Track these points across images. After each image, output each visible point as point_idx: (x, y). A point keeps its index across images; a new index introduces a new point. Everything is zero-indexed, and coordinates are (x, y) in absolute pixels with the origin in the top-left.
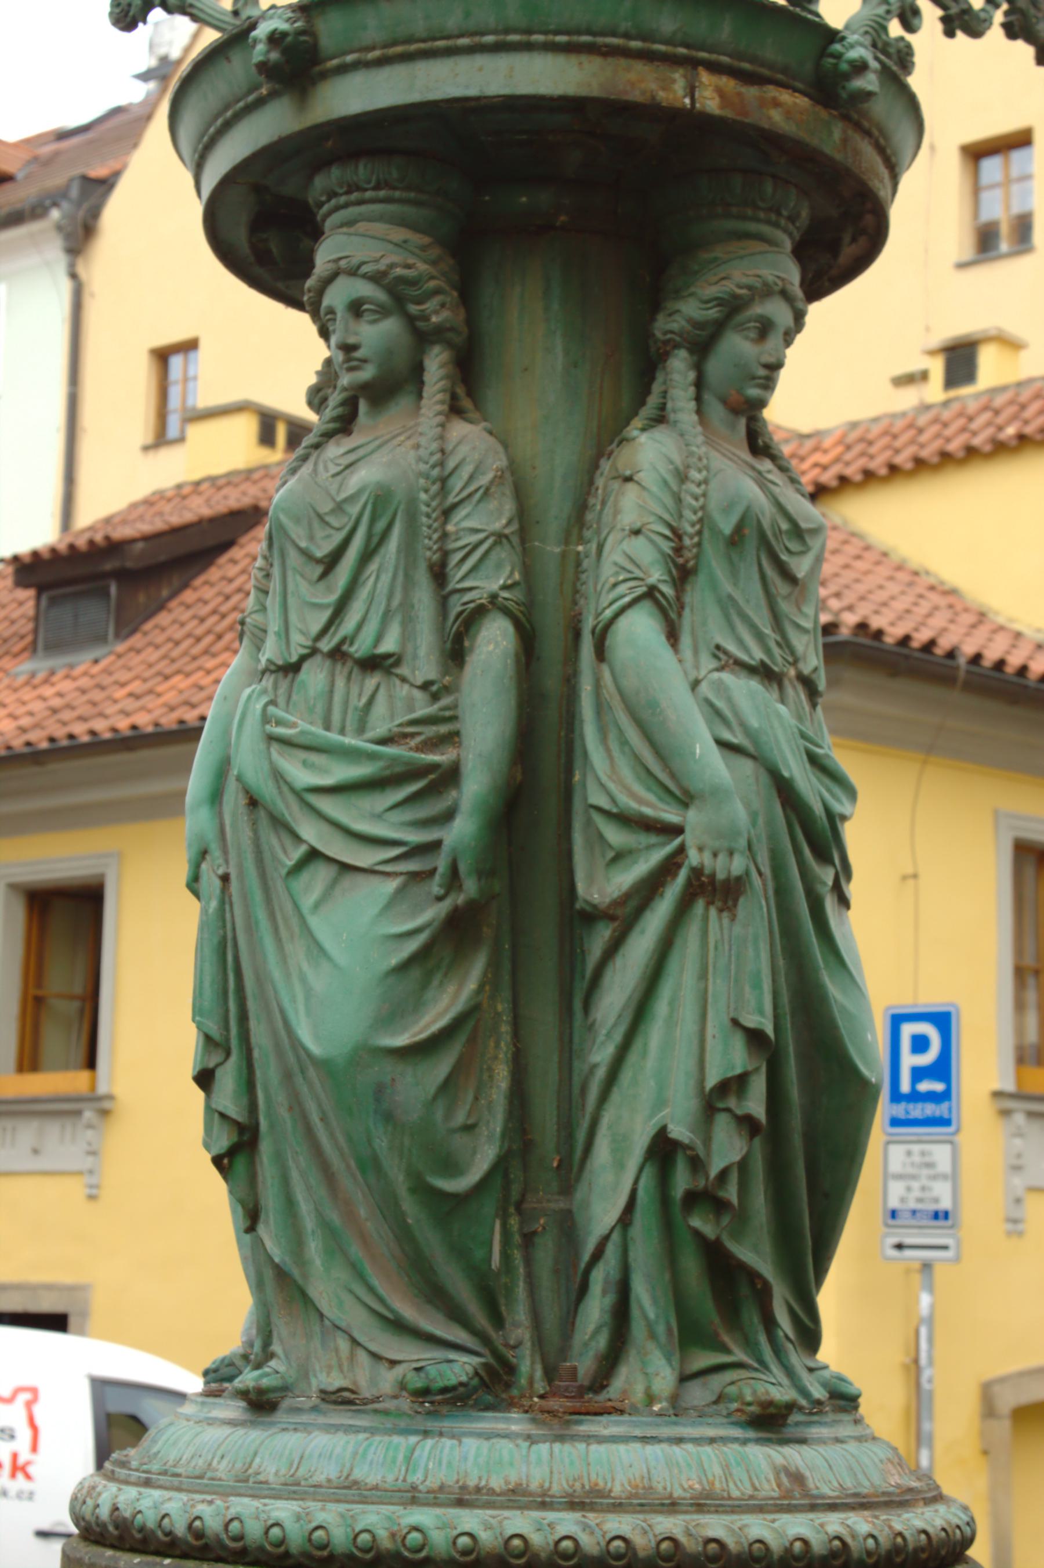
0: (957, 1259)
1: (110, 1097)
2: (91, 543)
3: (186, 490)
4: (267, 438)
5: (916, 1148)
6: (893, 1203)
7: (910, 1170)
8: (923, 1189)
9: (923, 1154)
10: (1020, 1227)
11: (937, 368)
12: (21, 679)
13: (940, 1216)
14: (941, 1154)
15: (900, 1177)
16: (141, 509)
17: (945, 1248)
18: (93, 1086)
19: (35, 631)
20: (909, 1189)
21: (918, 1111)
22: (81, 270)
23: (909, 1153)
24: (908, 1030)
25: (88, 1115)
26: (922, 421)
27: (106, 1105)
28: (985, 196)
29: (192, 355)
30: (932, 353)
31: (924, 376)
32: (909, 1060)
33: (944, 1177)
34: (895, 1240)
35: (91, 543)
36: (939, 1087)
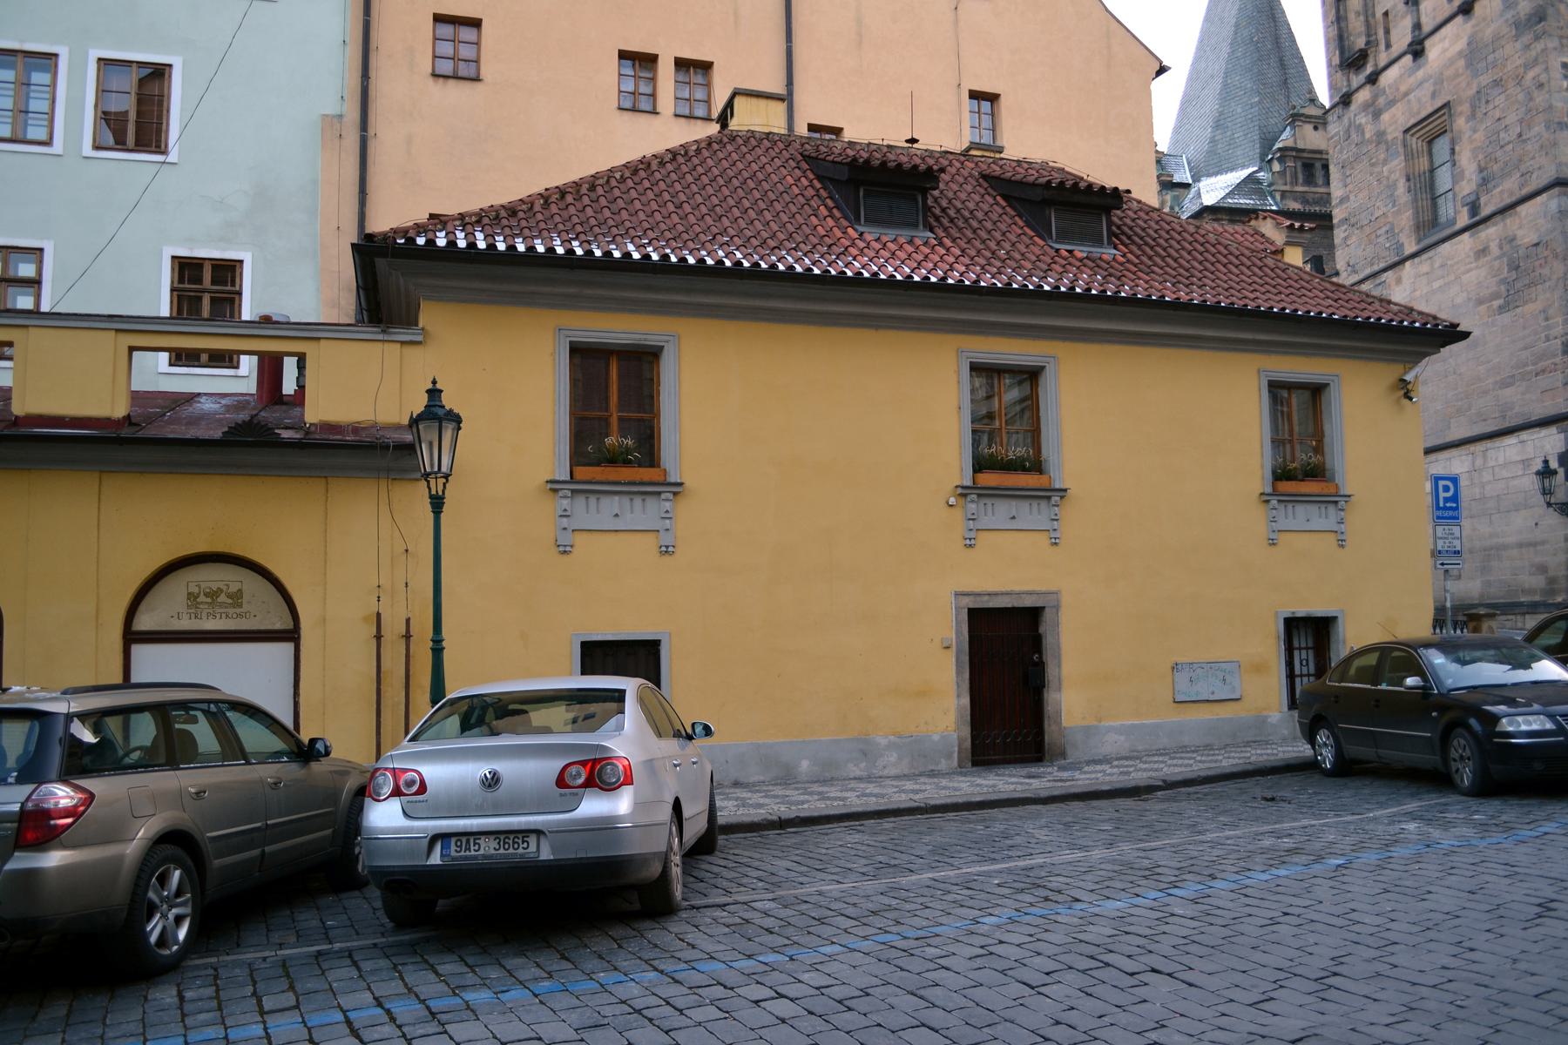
2: (884, 164)
6: (1439, 548)
14: (1456, 530)
15: (1441, 538)
24: (1441, 483)
32: (1442, 495)
35: (884, 164)
36: (1454, 505)
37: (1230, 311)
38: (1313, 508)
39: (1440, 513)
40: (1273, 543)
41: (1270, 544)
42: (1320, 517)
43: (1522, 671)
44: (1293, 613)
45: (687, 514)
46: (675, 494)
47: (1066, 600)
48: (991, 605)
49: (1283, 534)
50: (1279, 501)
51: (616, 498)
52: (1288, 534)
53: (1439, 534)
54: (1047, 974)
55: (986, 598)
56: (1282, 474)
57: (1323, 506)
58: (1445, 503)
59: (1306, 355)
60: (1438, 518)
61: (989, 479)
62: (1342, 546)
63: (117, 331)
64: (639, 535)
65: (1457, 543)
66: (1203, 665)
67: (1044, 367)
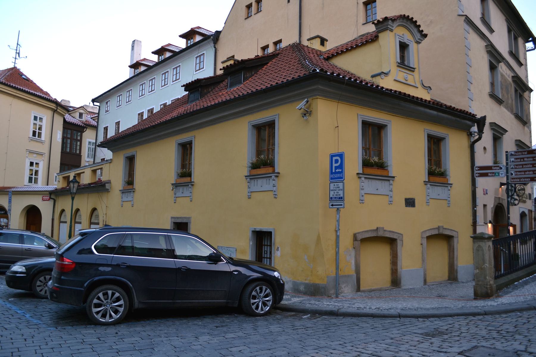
1: (193, 182)
5: (336, 184)
6: (331, 196)
7: (334, 189)
8: (337, 193)
9: (337, 185)
14: (341, 185)
17: (342, 205)
20: (334, 193)
21: (336, 176)
22: (216, 46)
23: (334, 185)
24: (334, 158)
27: (193, 183)
28: (368, 11)
32: (334, 165)
34: (332, 204)
36: (340, 170)
37: (235, 99)
39: (332, 176)
41: (249, 198)
43: (78, 252)
44: (255, 229)
45: (396, 184)
47: (192, 220)
49: (253, 193)
50: (250, 179)
51: (127, 193)
53: (332, 188)
56: (254, 166)
57: (268, 179)
58: (336, 169)
59: (267, 109)
60: (332, 179)
62: (275, 197)
63: (91, 167)
65: (341, 193)
66: (225, 248)
67: (275, 120)
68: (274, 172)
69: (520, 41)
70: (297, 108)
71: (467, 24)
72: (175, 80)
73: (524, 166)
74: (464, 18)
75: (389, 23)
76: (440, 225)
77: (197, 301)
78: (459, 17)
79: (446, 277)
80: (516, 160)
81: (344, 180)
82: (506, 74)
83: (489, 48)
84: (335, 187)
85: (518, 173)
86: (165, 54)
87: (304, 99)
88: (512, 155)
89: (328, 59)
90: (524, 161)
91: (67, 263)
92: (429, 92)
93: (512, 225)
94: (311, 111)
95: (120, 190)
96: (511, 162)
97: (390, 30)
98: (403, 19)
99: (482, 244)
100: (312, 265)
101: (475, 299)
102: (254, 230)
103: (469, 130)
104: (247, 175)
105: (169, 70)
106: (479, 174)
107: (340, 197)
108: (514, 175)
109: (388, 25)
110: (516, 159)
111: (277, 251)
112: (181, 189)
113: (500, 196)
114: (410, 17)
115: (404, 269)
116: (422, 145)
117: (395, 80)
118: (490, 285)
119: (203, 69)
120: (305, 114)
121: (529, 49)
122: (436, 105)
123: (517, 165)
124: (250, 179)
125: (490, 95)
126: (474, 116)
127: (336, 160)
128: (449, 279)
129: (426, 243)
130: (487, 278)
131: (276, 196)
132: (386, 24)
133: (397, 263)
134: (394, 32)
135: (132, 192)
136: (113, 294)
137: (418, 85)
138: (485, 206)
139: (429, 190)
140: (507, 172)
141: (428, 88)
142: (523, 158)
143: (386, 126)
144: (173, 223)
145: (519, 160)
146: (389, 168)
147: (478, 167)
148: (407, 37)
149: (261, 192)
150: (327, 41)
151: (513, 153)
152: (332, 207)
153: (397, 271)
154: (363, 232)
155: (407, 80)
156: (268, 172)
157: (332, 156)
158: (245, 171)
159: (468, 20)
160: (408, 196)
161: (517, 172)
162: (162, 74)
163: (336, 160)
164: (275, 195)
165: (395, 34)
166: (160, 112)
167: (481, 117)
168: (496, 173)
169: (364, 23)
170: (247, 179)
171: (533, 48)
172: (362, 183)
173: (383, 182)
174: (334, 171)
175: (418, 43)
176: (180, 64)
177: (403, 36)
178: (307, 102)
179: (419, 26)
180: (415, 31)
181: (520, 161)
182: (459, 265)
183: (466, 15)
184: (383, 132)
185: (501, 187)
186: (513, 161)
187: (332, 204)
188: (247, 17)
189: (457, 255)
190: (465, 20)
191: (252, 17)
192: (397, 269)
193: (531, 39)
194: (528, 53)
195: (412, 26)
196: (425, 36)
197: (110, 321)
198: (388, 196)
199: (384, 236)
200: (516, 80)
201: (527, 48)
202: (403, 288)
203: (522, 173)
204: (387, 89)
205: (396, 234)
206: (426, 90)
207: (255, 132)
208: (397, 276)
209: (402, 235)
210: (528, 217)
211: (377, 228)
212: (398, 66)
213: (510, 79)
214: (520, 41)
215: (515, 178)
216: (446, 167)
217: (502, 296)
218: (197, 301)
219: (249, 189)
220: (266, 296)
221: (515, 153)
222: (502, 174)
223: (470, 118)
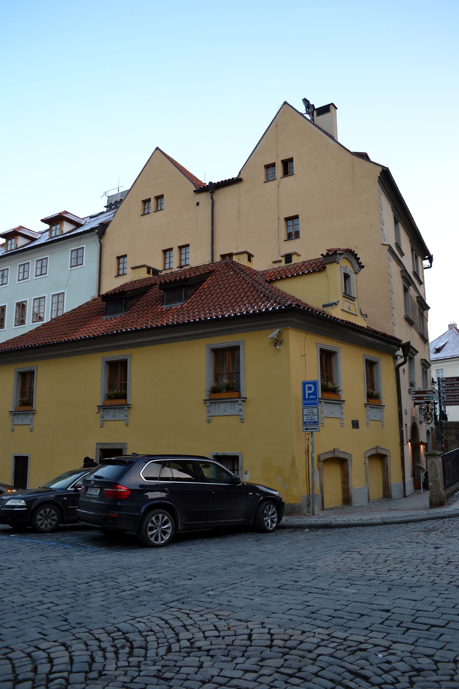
0: (319, 431)
1: (130, 404)
2: (119, 292)
3: (133, 282)
4: (149, 272)
8: (311, 417)
9: (311, 410)
10: (323, 425)
11: (283, 259)
12: (104, 320)
13: (316, 423)
14: (315, 410)
15: (306, 415)
16: (123, 286)
17: (317, 429)
18: (126, 403)
19: (106, 309)
20: (308, 418)
21: (309, 402)
22: (102, 242)
23: (308, 410)
24: (307, 386)
25: (240, 402)
26: (275, 271)
27: (129, 406)
29: (125, 258)
30: (282, 257)
31: (280, 261)
32: (307, 392)
33: (316, 415)
35: (119, 292)
36: (314, 397)
38: (228, 405)
39: (306, 402)
40: (209, 421)
42: (231, 408)
44: (217, 453)
45: (345, 406)
46: (33, 413)
48: (106, 448)
50: (210, 403)
52: (214, 417)
53: (305, 413)
54: (117, 594)
55: (105, 445)
56: (214, 391)
58: (309, 396)
60: (305, 404)
61: (216, 396)
62: (242, 422)
64: (26, 426)
65: (316, 418)
68: (240, 397)
69: (419, 259)
70: (269, 337)
71: (389, 252)
72: (40, 274)
73: (454, 391)
74: (387, 247)
75: (338, 257)
76: (378, 445)
77: (224, 521)
78: (383, 246)
79: (381, 495)
80: (447, 386)
81: (318, 406)
82: (413, 295)
83: (404, 273)
84: (309, 412)
85: (450, 397)
86: (17, 238)
87: (277, 328)
88: (443, 381)
89: (271, 281)
90: (454, 387)
91: (123, 490)
92: (366, 319)
93: (422, 443)
94: (282, 341)
95: (10, 412)
96: (442, 387)
97: (337, 263)
98: (349, 254)
99: (434, 460)
100: (287, 486)
101: (431, 508)
102: (216, 455)
103: (394, 354)
104: (205, 399)
105: (30, 261)
106: (415, 397)
107: (314, 422)
108: (445, 399)
109: (337, 258)
110: (447, 385)
111: (245, 475)
112: (112, 412)
113: (414, 415)
114: (353, 250)
115: (354, 488)
116: (362, 368)
117: (342, 310)
118: (443, 495)
119: (82, 266)
120: (276, 343)
121: (425, 267)
122: (363, 329)
123: (448, 390)
124: (210, 403)
125: (405, 318)
126: (400, 341)
127: (308, 387)
128: (384, 496)
129: (368, 463)
130: (440, 489)
131: (243, 420)
132: (334, 257)
133: (348, 482)
134: (340, 264)
135: (31, 414)
136: (163, 517)
137: (358, 313)
138: (406, 425)
139: (368, 412)
140: (440, 396)
141: (365, 316)
142: (453, 384)
143: (336, 352)
144: (99, 449)
145: (450, 386)
146: (340, 393)
147: (415, 392)
148: (350, 270)
149: (223, 417)
150: (253, 256)
151: (444, 379)
152: (306, 430)
153: (349, 490)
154: (324, 453)
155: (350, 310)
156: (233, 396)
157: (304, 384)
158: (204, 395)
159: (391, 250)
160: (354, 419)
161: (448, 396)
162: (20, 266)
163: (308, 387)
164: (242, 419)
165: (341, 266)
166: (62, 321)
167: (406, 343)
168: (430, 397)
169: (285, 239)
170: (206, 403)
171: (430, 266)
172: (322, 408)
173: (336, 405)
174: (307, 397)
175: (356, 273)
176: (48, 256)
177: (346, 268)
178: (280, 332)
179: (359, 258)
180: (355, 262)
181: (451, 387)
182: (392, 483)
183: (390, 245)
184: (333, 357)
185: (414, 407)
186: (444, 387)
187: (306, 428)
188: (142, 214)
189: (390, 474)
190: (388, 250)
191: (150, 214)
192: (349, 488)
193: (427, 257)
194: (425, 270)
195: (353, 258)
196: (363, 267)
197: (162, 542)
198: (340, 419)
199: (338, 456)
200: (420, 301)
201: (424, 266)
202: (354, 505)
203: (453, 397)
204: (341, 320)
205: (347, 455)
206: (363, 318)
207: (213, 355)
208: (349, 495)
209: (351, 455)
210: (431, 434)
211: (334, 449)
212: (344, 296)
213: (415, 300)
214: (419, 259)
215: (446, 402)
216: (379, 390)
217: (453, 504)
218: (224, 521)
219: (208, 413)
220: (272, 515)
221: (446, 380)
222: (435, 398)
223: (396, 342)
